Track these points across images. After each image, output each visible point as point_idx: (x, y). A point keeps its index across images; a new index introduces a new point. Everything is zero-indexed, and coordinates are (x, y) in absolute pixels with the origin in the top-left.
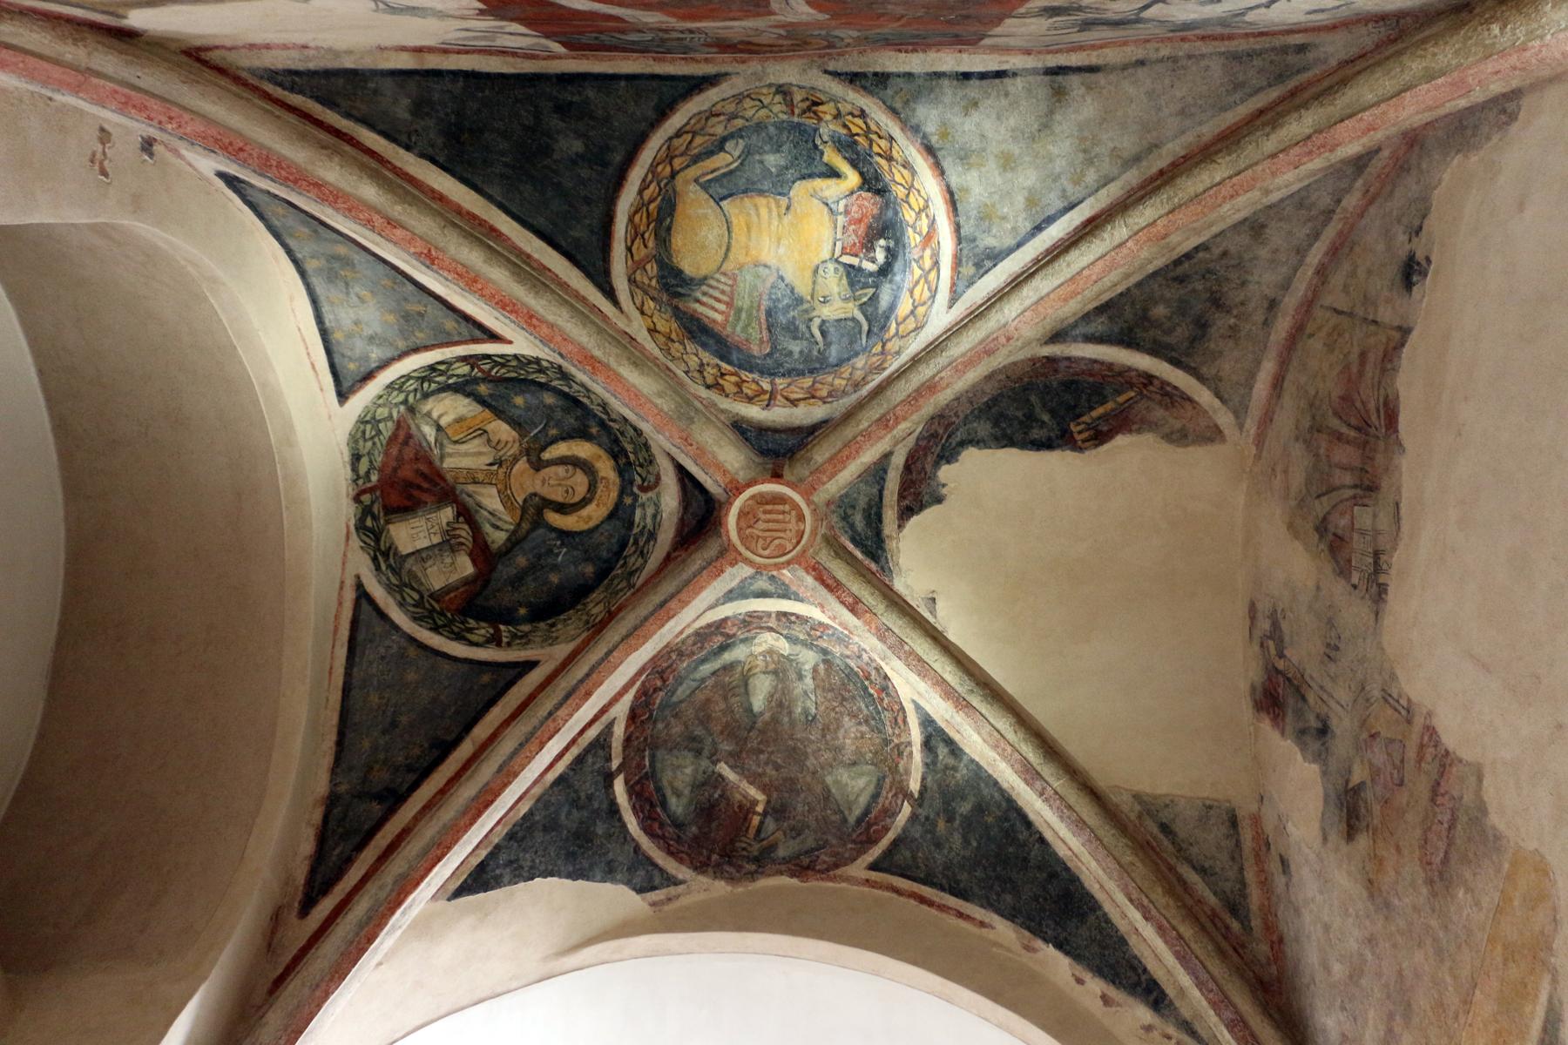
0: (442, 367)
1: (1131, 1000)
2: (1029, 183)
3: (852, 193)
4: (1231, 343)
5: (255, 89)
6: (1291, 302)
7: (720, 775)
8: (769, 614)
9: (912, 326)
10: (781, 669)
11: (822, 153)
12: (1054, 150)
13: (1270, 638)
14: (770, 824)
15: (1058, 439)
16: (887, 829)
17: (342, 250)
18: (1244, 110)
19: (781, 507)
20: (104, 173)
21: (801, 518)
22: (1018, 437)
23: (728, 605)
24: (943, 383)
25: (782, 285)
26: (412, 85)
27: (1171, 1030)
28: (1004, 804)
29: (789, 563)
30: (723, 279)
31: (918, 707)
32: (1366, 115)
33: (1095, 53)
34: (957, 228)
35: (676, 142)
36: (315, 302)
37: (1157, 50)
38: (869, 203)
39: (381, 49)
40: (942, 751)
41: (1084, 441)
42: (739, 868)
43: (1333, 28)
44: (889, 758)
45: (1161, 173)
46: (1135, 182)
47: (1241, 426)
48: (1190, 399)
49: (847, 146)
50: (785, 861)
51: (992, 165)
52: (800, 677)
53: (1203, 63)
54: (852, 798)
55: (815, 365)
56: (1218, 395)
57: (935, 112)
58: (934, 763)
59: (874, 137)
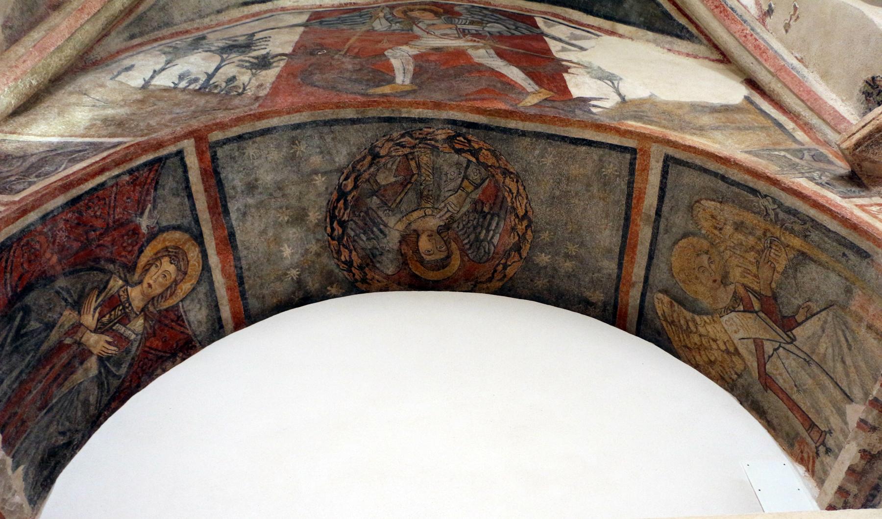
5: (702, 32)
20: (795, 8)
26: (621, 14)
32: (86, 17)
33: (246, 13)
37: (207, 102)
39: (631, 39)
43: (118, 53)
53: (184, 18)
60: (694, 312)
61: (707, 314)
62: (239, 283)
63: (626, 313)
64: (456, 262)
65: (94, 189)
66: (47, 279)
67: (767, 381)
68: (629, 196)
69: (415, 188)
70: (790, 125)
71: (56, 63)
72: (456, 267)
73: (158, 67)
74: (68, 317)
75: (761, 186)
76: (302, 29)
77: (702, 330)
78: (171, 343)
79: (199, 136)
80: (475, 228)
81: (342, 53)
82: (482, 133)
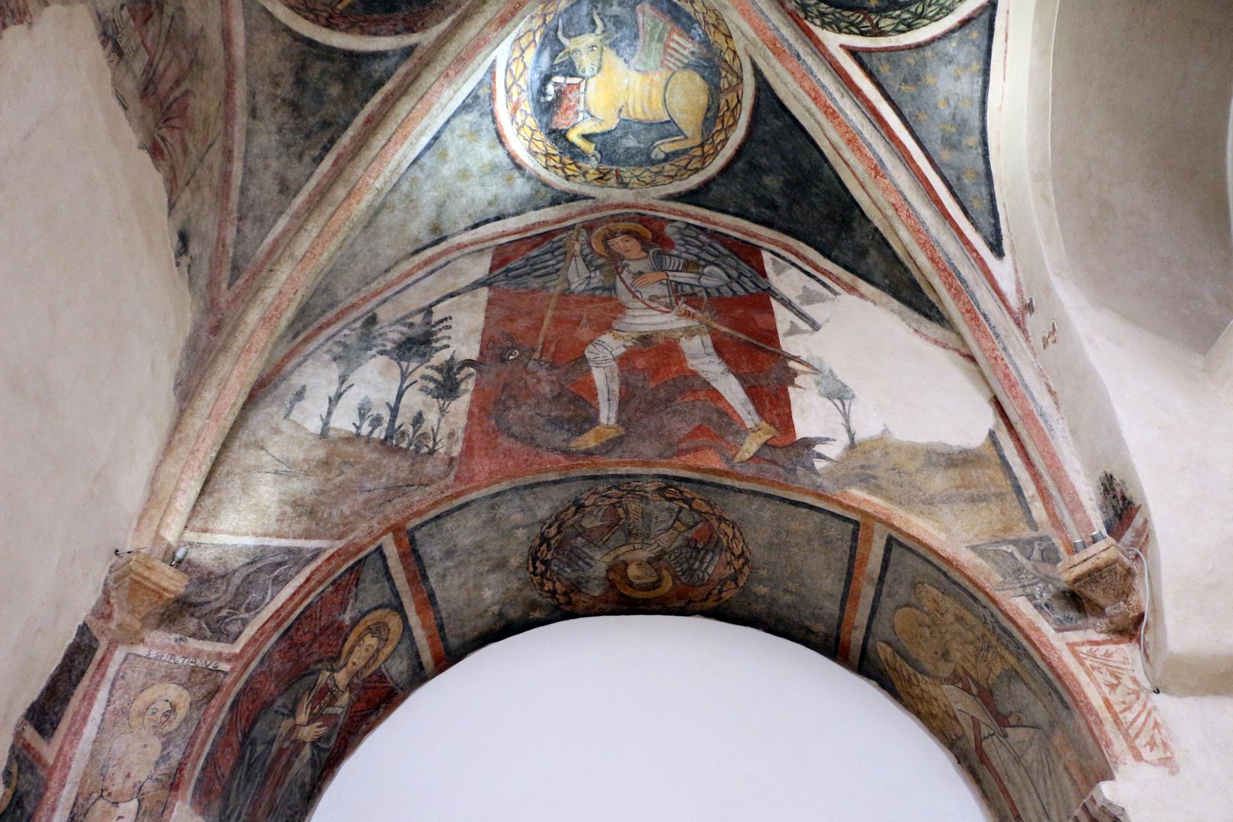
0: (902, 27)
6: (241, 118)
17: (945, 156)
20: (1054, 330)
26: (863, 269)
34: (494, 120)
35: (698, 165)
36: (984, 103)
38: (560, 122)
48: (292, 8)
49: (575, 153)
56: (270, 15)
60: (916, 669)
61: (929, 676)
62: (439, 630)
63: (848, 647)
64: (667, 585)
65: (303, 612)
66: (268, 705)
67: (983, 758)
68: (852, 557)
69: (620, 526)
70: (1030, 490)
72: (668, 589)
73: (332, 391)
74: (286, 724)
75: (980, 596)
76: (484, 293)
77: (924, 687)
78: (378, 699)
79: (396, 529)
80: (688, 559)
81: (537, 355)
82: (694, 486)
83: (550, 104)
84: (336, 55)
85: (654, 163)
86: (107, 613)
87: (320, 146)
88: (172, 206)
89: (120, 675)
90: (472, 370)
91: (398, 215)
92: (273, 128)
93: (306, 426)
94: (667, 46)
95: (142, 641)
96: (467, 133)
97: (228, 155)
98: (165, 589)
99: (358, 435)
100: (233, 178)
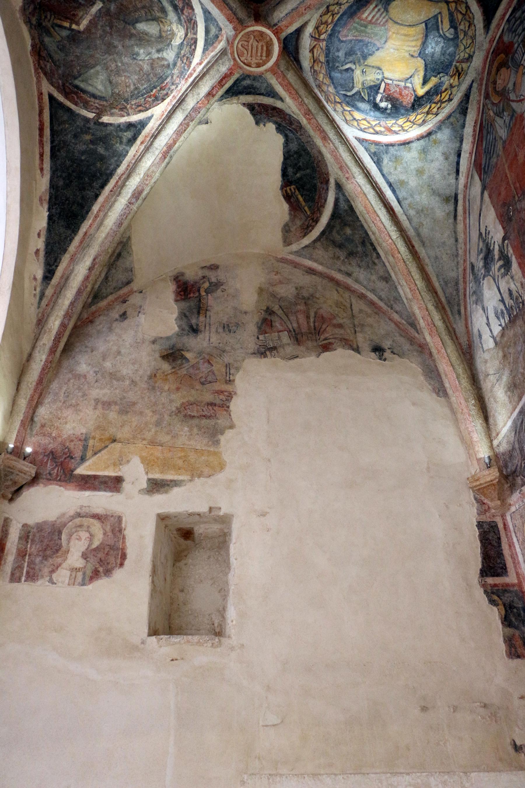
1: (42, 265)
2: (410, 183)
3: (414, 91)
4: (332, 256)
6: (349, 281)
7: (94, 3)
8: (196, 33)
9: (348, 119)
10: (163, 40)
11: (435, 77)
12: (424, 196)
13: (211, 283)
14: (65, 33)
15: (287, 179)
16: (76, 104)
18: (437, 285)
19: (264, 54)
21: (258, 66)
22: (288, 162)
23: (201, 10)
24: (327, 144)
25: (374, 49)
27: (38, 289)
28: (108, 172)
29: (234, 59)
30: (384, 20)
31: (150, 118)
33: (462, 219)
34: (392, 145)
35: (463, 6)
38: (408, 100)
40: (128, 135)
41: (286, 191)
42: (32, 14)
44: (119, 103)
45: (413, 247)
46: (409, 233)
47: (291, 253)
48: (305, 236)
50: (42, 42)
51: (420, 164)
52: (158, 51)
53: (455, 268)
54: (90, 82)
55: (331, 64)
56: (306, 247)
57: (446, 138)
58: (121, 130)
59: (439, 105)
71: (465, 383)
81: (517, 198)
83: (394, 106)
84: (332, 224)
85: (456, 37)
86: (487, 508)
87: (372, 251)
88: (357, 350)
89: (515, 526)
90: (506, 242)
91: (427, 222)
92: (358, 269)
93: (490, 347)
94: (370, 22)
95: (510, 505)
96: (394, 165)
97: (362, 296)
98: (491, 481)
99: (503, 329)
100: (374, 300)
